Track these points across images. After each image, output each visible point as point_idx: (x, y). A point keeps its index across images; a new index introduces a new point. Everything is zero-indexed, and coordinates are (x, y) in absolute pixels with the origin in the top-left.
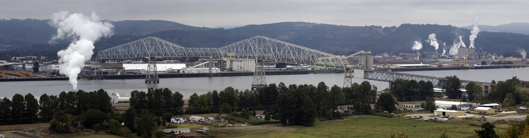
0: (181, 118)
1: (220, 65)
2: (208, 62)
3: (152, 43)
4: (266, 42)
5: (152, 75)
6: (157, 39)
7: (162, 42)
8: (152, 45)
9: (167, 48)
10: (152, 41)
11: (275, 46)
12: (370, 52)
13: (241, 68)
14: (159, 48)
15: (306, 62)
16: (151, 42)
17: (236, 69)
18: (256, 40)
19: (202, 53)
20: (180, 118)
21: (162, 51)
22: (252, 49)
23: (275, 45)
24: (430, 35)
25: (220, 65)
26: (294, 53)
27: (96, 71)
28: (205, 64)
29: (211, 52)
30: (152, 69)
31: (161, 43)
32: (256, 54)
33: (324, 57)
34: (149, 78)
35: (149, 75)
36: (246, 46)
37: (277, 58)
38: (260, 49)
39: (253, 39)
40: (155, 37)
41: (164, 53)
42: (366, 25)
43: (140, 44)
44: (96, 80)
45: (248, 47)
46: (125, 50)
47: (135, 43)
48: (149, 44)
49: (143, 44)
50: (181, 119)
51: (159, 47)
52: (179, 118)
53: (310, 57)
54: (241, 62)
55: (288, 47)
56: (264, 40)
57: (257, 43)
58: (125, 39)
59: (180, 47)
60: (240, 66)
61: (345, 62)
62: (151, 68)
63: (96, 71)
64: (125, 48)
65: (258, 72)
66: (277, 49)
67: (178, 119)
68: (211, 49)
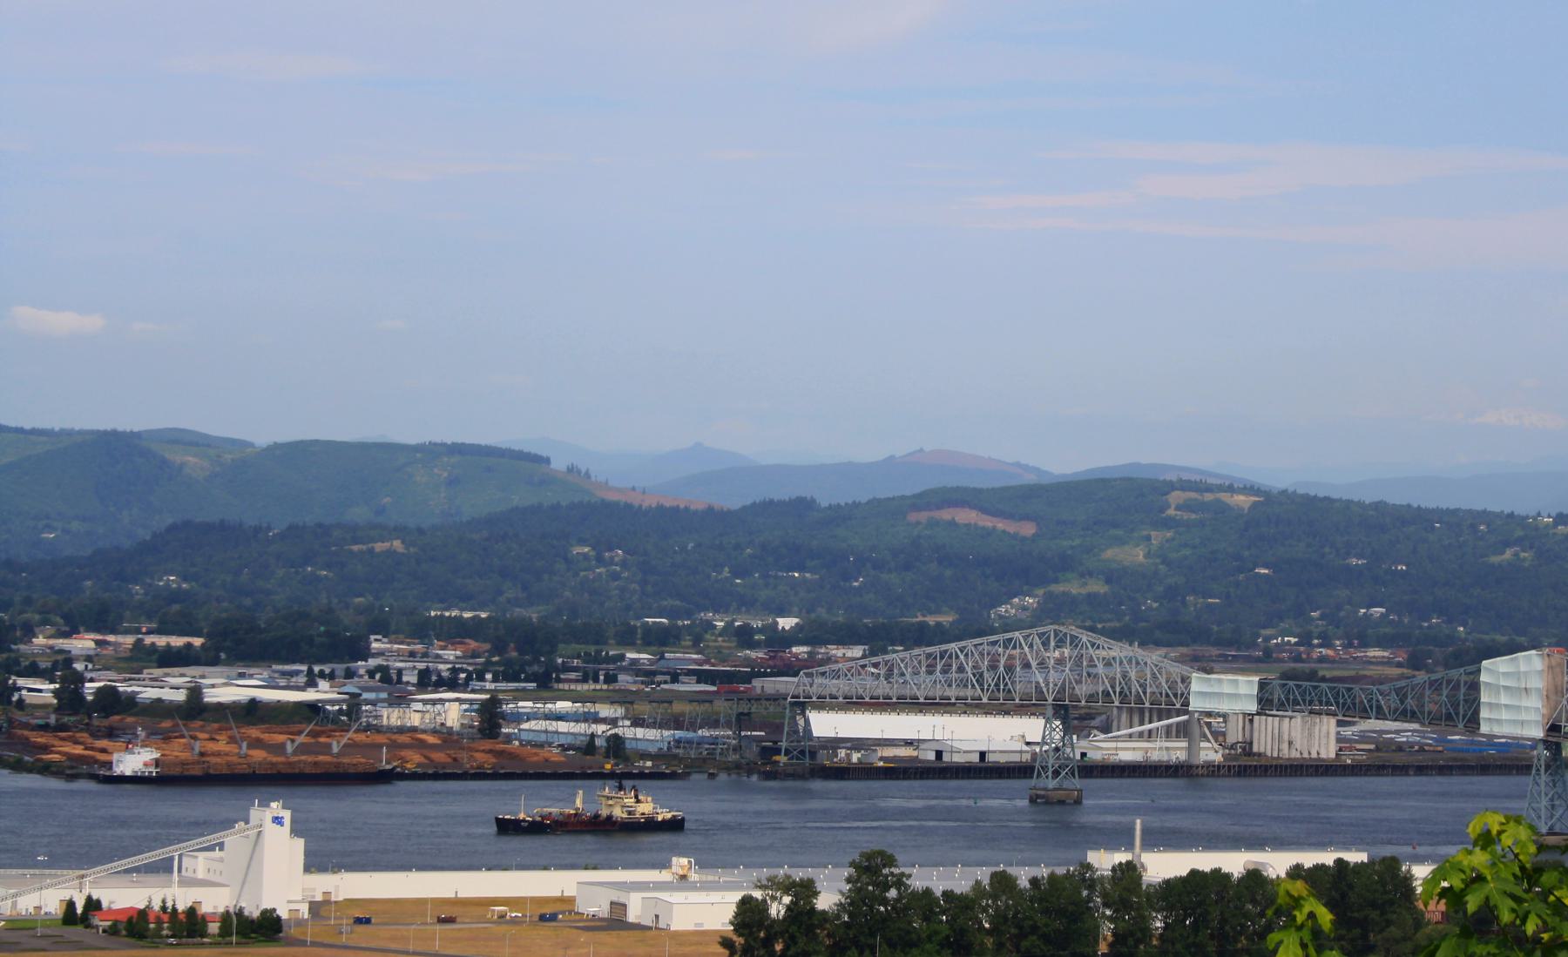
13: (1290, 743)
17: (1269, 747)
24: (1494, 671)
28: (1169, 727)
30: (1057, 730)
37: (988, 690)
58: (387, 545)
60: (1286, 737)
62: (1054, 727)
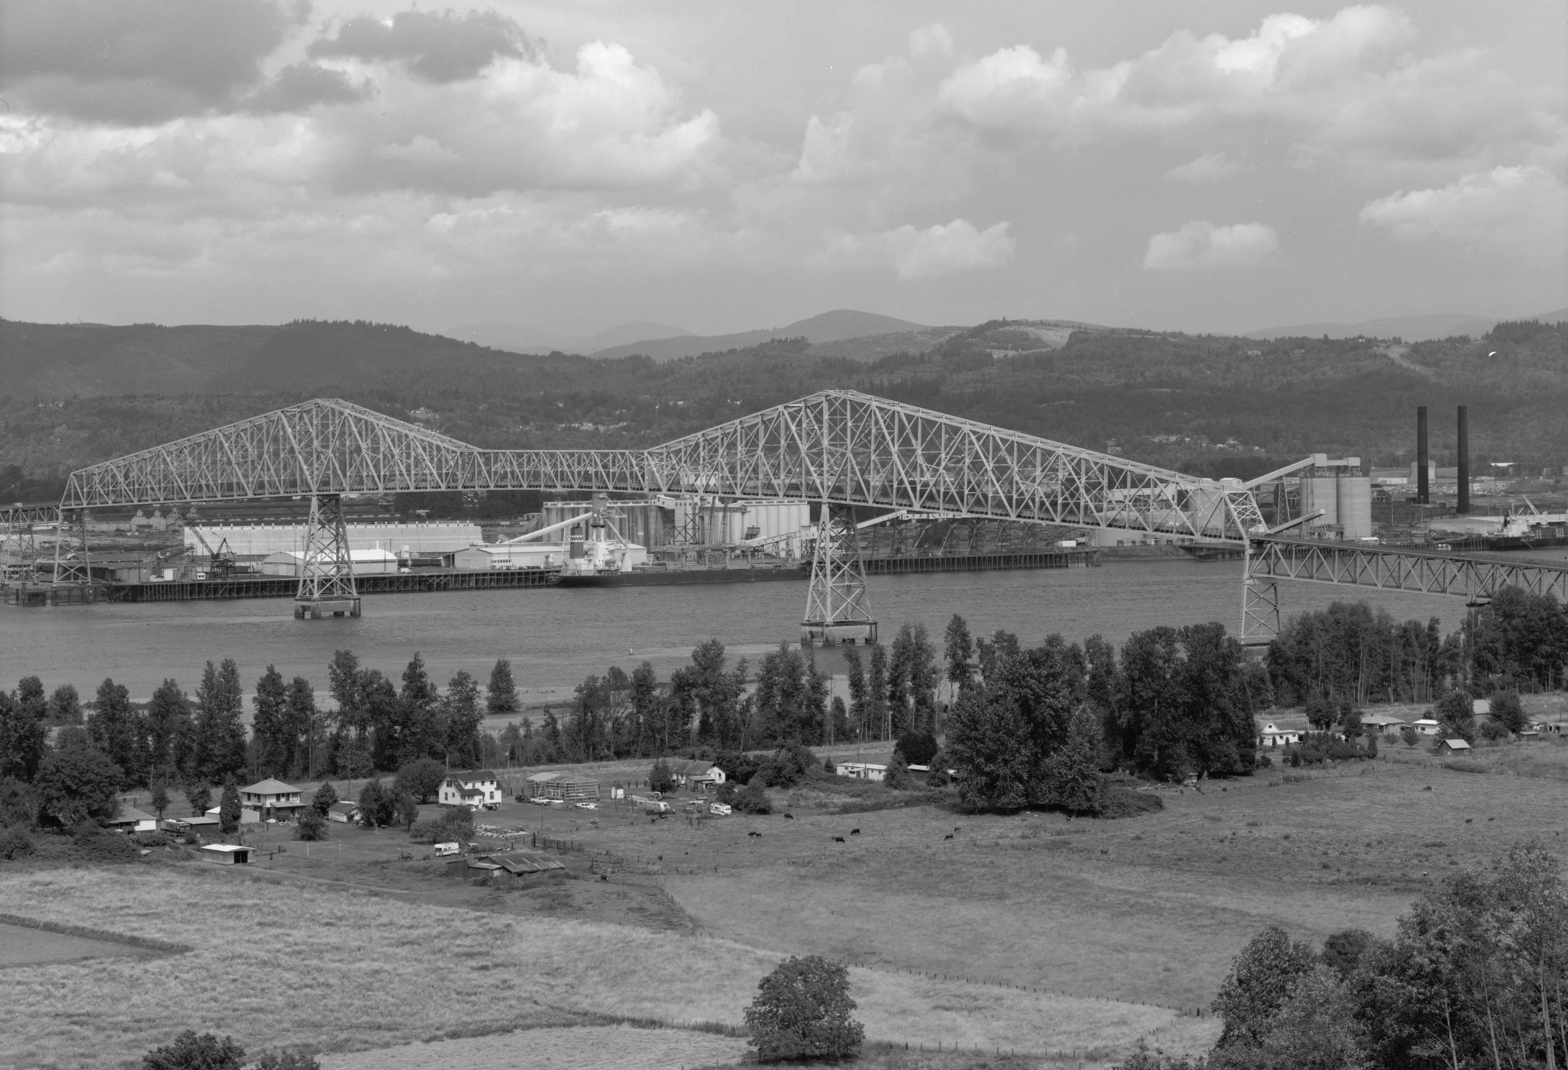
0: (487, 784)
1: (646, 530)
2: (589, 514)
3: (325, 426)
4: (870, 416)
5: (327, 581)
6: (349, 410)
7: (375, 422)
8: (326, 439)
9: (396, 452)
10: (325, 417)
11: (911, 436)
12: (1355, 462)
14: (358, 450)
15: (1059, 508)
16: (322, 425)
18: (821, 412)
19: (562, 472)
20: (483, 783)
21: (376, 467)
22: (803, 455)
23: (908, 430)
25: (646, 530)
26: (1001, 469)
27: (59, 565)
29: (605, 466)
31: (369, 428)
32: (821, 474)
33: (1144, 487)
34: (311, 594)
35: (312, 581)
36: (773, 439)
38: (842, 450)
39: (807, 407)
40: (341, 401)
41: (382, 473)
42: (1326, 336)
43: (268, 433)
44: (60, 608)
45: (783, 442)
46: (200, 464)
47: (245, 431)
48: (314, 434)
49: (281, 433)
50: (488, 788)
51: (292, 448)
52: (478, 785)
53: (1077, 489)
54: (743, 513)
55: (971, 443)
56: (856, 406)
57: (825, 425)
59: (459, 447)
61: (1246, 509)
63: (59, 565)
64: (200, 453)
65: (832, 563)
66: (919, 452)
67: (469, 786)
68: (607, 455)
